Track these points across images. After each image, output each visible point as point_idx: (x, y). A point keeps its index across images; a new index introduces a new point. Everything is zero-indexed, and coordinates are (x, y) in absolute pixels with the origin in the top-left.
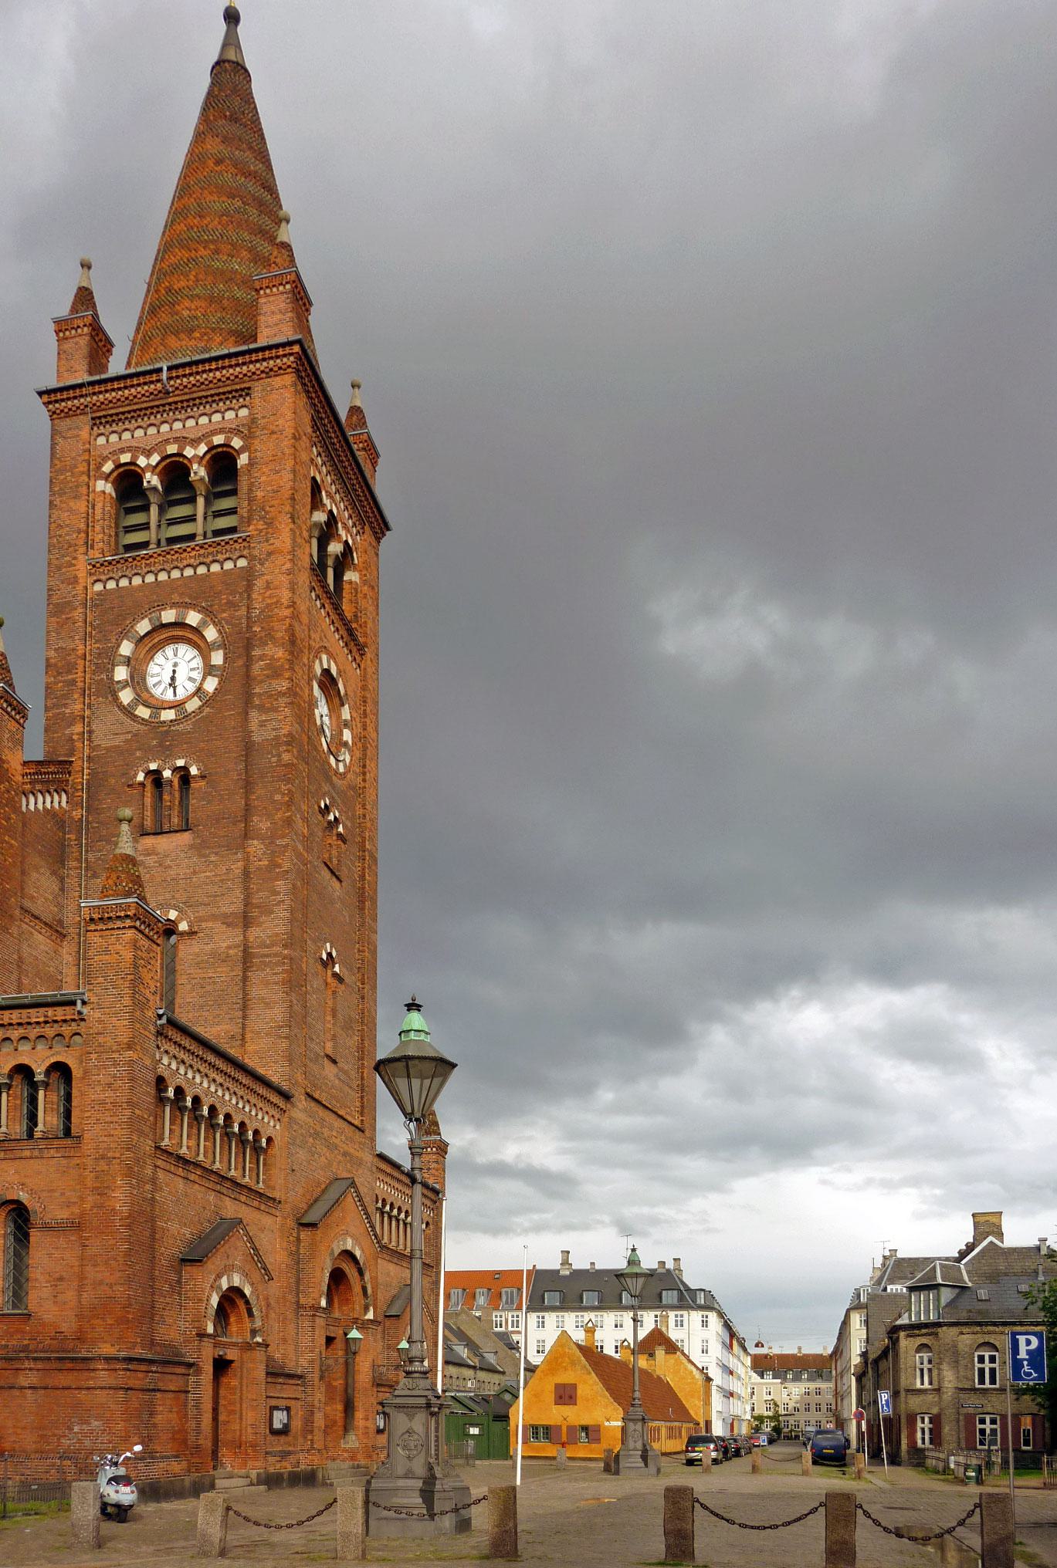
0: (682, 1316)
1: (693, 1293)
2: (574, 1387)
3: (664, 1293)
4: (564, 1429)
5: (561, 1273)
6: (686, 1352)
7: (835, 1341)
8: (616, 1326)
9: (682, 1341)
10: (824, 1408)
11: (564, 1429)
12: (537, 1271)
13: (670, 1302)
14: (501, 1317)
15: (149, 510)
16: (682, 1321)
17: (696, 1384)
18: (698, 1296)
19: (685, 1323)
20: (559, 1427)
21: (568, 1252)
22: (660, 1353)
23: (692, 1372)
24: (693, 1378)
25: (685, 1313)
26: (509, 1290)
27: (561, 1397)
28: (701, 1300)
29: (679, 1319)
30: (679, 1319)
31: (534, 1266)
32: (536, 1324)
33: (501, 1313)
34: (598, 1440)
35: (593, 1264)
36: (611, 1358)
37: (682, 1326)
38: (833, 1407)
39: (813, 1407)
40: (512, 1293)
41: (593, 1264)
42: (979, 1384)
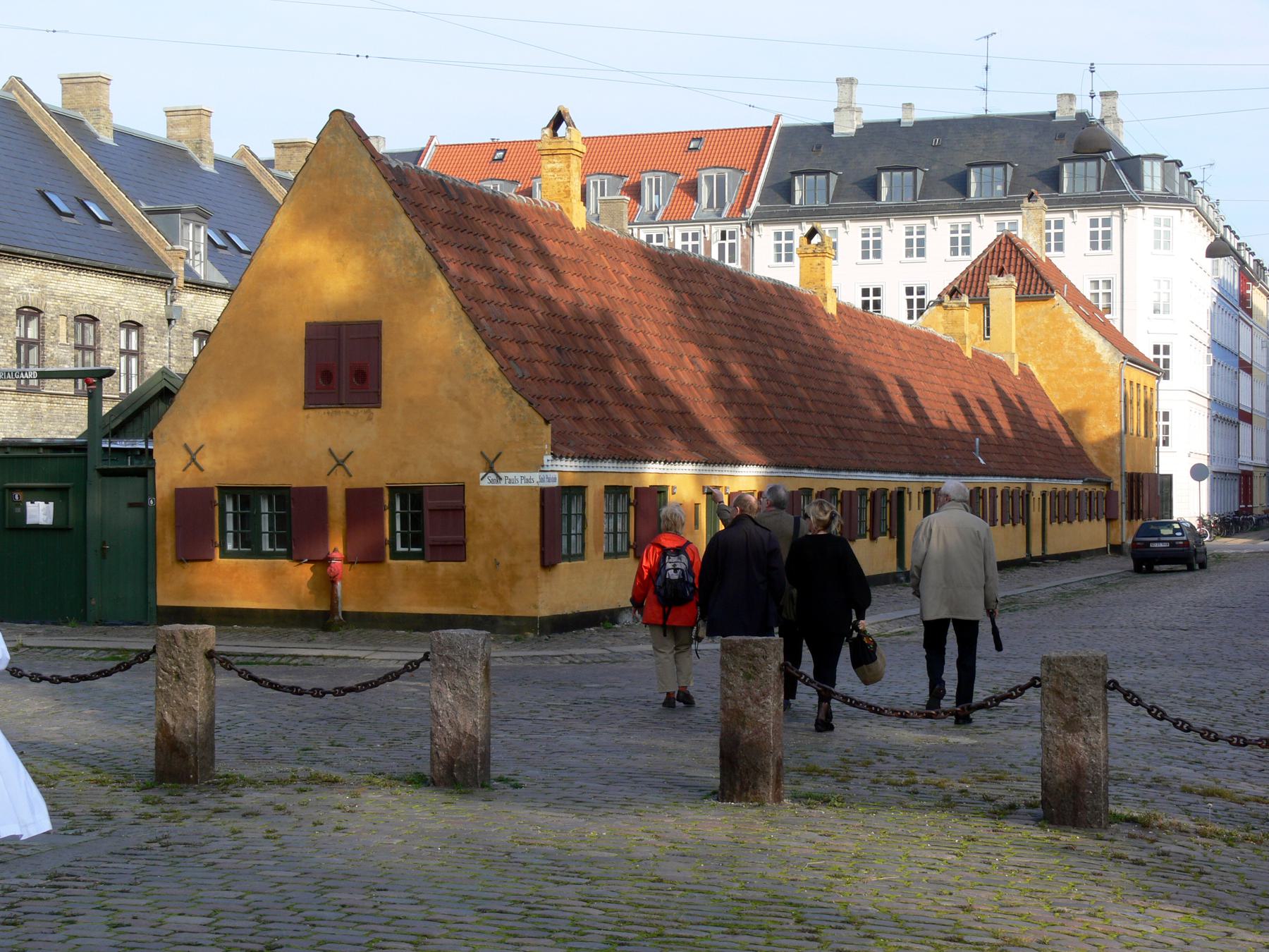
0: (1107, 222)
1: (1132, 165)
3: (1066, 170)
4: (337, 507)
5: (838, 131)
8: (1156, 311)
9: (1108, 283)
13: (1080, 190)
14: (695, 237)
16: (1107, 235)
17: (1102, 378)
21: (851, 81)
22: (1002, 290)
23: (1093, 347)
24: (1096, 361)
26: (714, 173)
28: (1152, 179)
31: (778, 118)
32: (772, 253)
33: (696, 229)
34: (455, 550)
37: (1107, 246)
40: (721, 181)
41: (908, 106)
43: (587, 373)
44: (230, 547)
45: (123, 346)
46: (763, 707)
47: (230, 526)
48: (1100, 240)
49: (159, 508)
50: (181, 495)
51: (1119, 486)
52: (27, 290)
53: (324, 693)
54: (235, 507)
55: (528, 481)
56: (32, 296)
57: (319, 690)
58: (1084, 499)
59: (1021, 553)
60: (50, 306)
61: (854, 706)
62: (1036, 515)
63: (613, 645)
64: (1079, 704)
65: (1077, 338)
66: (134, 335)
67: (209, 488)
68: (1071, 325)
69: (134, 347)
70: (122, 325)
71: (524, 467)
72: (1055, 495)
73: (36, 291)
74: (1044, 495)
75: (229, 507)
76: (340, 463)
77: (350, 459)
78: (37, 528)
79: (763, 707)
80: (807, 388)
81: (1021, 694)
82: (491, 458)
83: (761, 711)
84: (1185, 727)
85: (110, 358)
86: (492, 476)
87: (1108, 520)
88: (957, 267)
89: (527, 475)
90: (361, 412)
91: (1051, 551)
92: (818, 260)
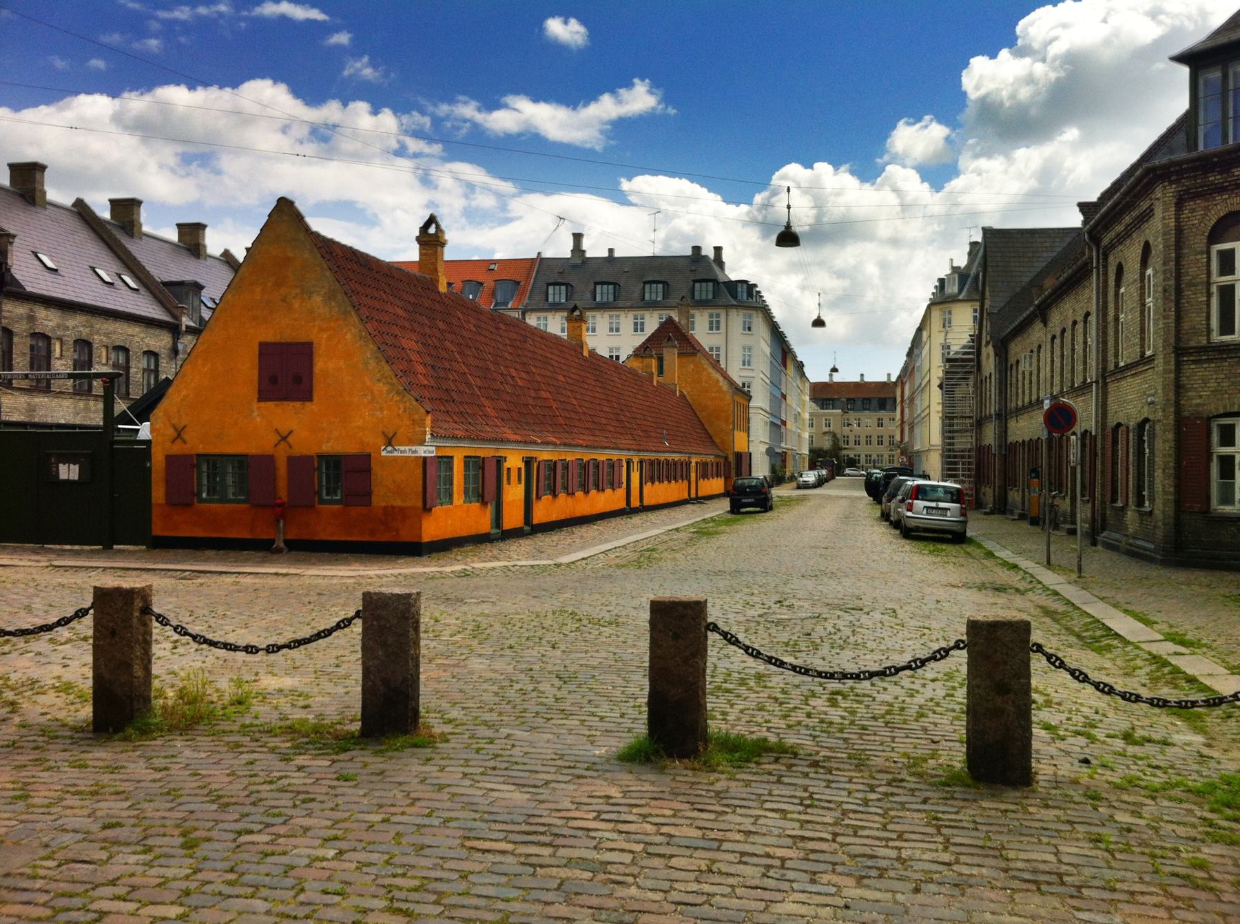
0: (718, 316)
2: (305, 351)
4: (282, 469)
6: (723, 366)
7: (903, 359)
9: (718, 349)
10: (886, 440)
11: (282, 469)
12: (542, 259)
15: (810, 451)
16: (718, 322)
18: (739, 289)
19: (723, 325)
20: (267, 461)
23: (718, 381)
24: (720, 390)
25: (723, 313)
27: (273, 380)
29: (714, 319)
30: (714, 319)
35: (611, 251)
36: (556, 337)
37: (718, 328)
38: (898, 438)
39: (874, 439)
42: (327, 495)
43: (450, 383)
44: (204, 495)
45: (145, 367)
46: (693, 666)
47: (205, 482)
48: (714, 326)
49: (153, 469)
50: (170, 459)
51: (731, 458)
52: (82, 329)
53: (258, 650)
54: (208, 469)
55: (413, 452)
56: (84, 332)
57: (252, 647)
58: (679, 467)
59: (686, 496)
60: (96, 339)
61: (779, 666)
62: (693, 475)
63: (473, 562)
64: (1008, 667)
65: (709, 377)
66: (152, 361)
67: (308, 457)
68: (706, 370)
69: (152, 367)
70: (145, 353)
71: (411, 442)
72: (652, 463)
73: (87, 330)
74: (697, 463)
75: (205, 468)
76: (284, 438)
77: (280, 431)
78: (68, 482)
79: (693, 666)
80: (576, 399)
81: (935, 652)
82: (390, 435)
83: (691, 670)
84: (1106, 689)
85: (136, 373)
86: (389, 448)
87: (726, 478)
88: (640, 340)
89: (413, 448)
90: (298, 404)
91: (700, 494)
92: (577, 325)
